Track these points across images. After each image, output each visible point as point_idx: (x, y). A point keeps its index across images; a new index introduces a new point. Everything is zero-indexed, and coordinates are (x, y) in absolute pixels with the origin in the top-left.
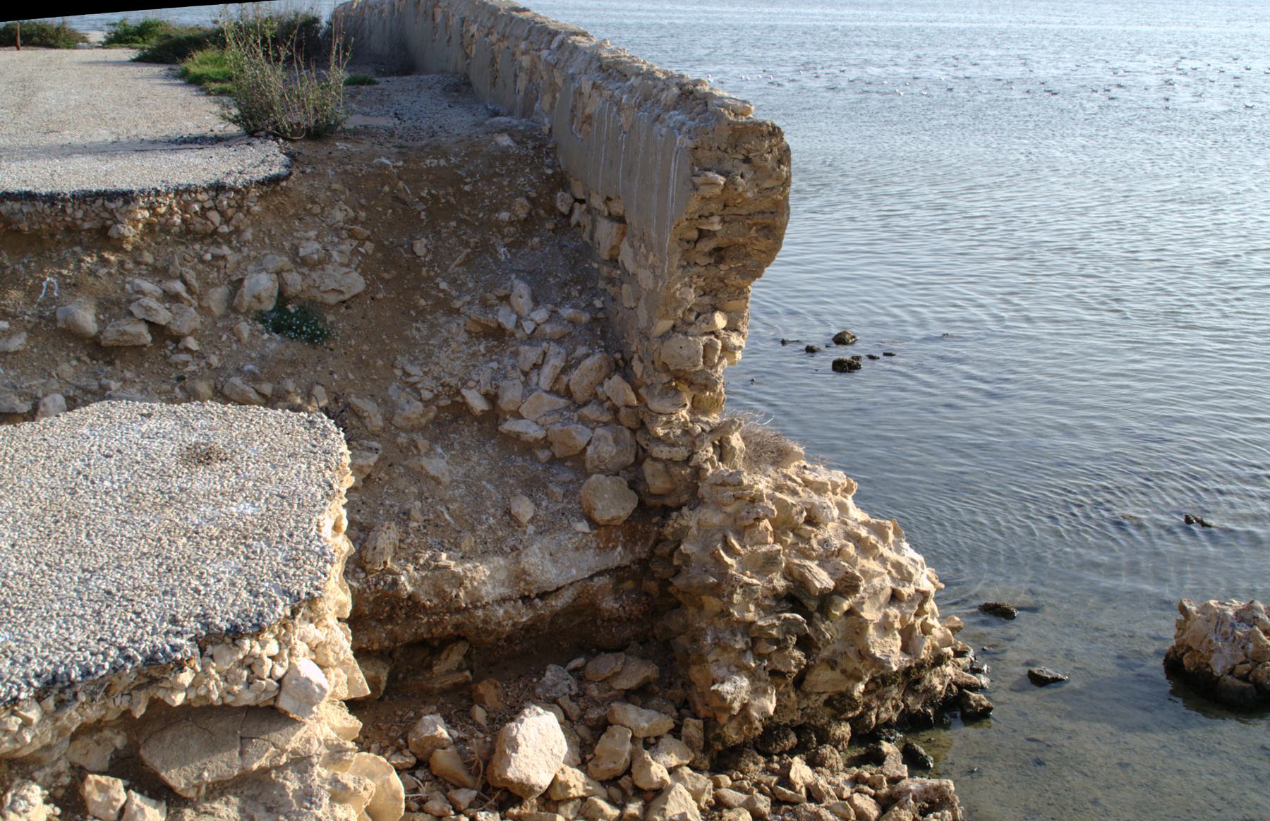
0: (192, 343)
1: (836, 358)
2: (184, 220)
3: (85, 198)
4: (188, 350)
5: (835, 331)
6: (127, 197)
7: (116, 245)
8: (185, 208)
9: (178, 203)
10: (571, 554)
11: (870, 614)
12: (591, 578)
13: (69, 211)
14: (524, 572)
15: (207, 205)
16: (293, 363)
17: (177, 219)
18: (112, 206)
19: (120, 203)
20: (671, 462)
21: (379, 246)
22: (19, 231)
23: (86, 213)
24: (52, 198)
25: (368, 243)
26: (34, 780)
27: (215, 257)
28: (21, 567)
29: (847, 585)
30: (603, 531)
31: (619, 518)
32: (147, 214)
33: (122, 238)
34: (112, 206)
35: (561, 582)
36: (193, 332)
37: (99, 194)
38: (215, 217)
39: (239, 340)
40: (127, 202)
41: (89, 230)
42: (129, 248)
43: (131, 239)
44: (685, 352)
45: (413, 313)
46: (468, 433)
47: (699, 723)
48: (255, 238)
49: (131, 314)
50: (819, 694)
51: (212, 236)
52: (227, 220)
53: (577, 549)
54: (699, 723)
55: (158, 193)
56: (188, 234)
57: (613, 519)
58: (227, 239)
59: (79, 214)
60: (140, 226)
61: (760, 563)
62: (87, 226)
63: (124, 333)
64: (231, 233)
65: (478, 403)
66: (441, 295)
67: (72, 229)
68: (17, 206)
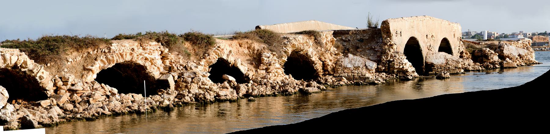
0: (351, 41)
1: (416, 36)
3: (347, 30)
5: (423, 42)
6: (350, 30)
7: (349, 34)
8: (355, 32)
11: (396, 63)
20: (384, 51)
21: (372, 36)
24: (345, 30)
26: (378, 65)
28: (307, 40)
29: (393, 61)
33: (349, 34)
36: (352, 40)
38: (358, 32)
46: (372, 50)
51: (357, 34)
56: (355, 34)
65: (373, 47)
67: (346, 33)
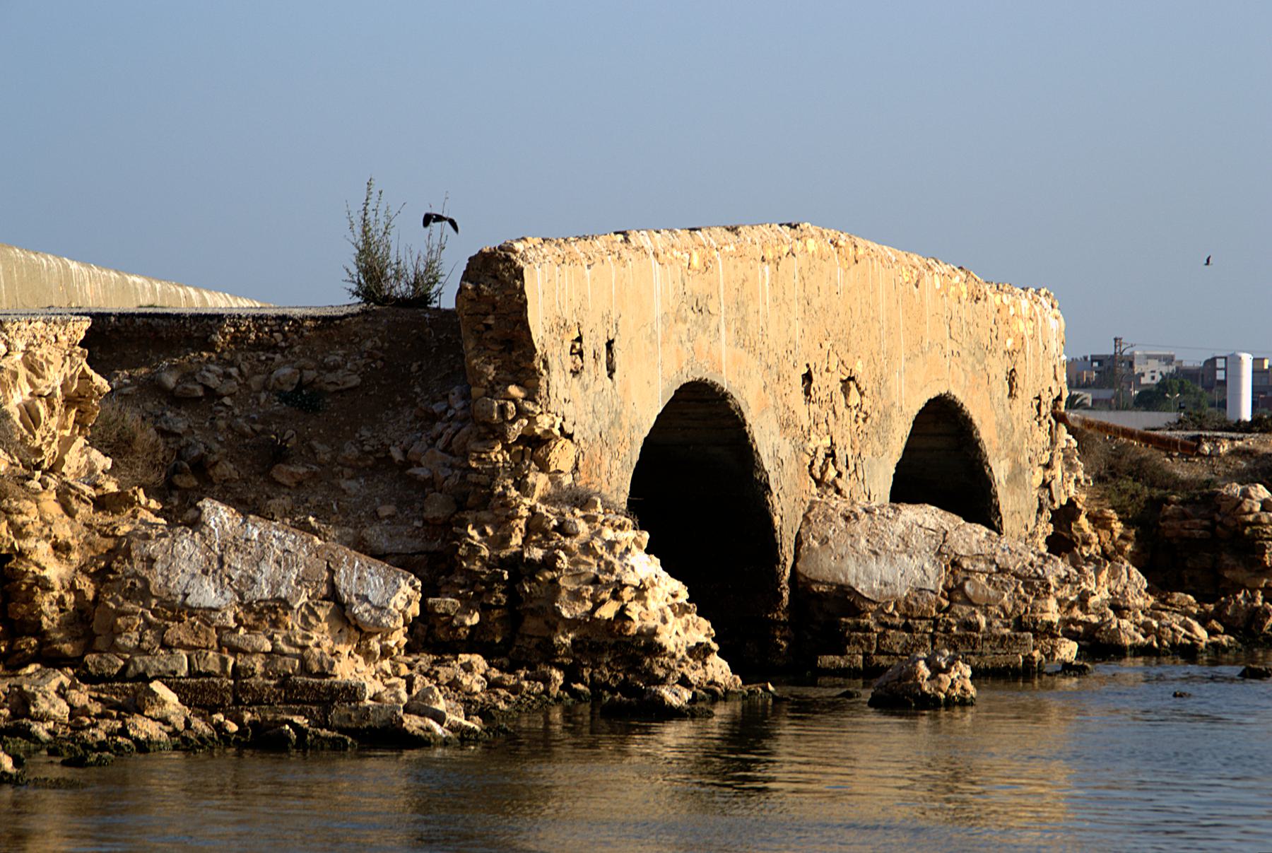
0: (227, 401)
2: (257, 336)
3: (198, 318)
4: (224, 405)
6: (219, 318)
7: (211, 347)
8: (259, 329)
9: (254, 326)
10: (404, 539)
12: (413, 554)
13: (188, 325)
14: (363, 539)
15: (274, 328)
16: (282, 417)
17: (253, 336)
18: (211, 323)
19: (216, 321)
22: (162, 338)
23: (197, 327)
25: (379, 362)
27: (267, 359)
30: (431, 528)
31: (439, 518)
32: (232, 330)
33: (214, 344)
34: (211, 323)
35: (389, 550)
36: (231, 395)
37: (206, 316)
39: (258, 404)
40: (219, 321)
41: (197, 338)
42: (219, 350)
43: (220, 343)
44: (485, 408)
45: (390, 405)
47: (426, 627)
48: (301, 351)
49: (195, 380)
50: (531, 637)
51: (274, 348)
52: (285, 338)
53: (411, 537)
54: (426, 627)
55: (240, 317)
56: (259, 345)
57: (434, 519)
58: (282, 350)
59: (194, 328)
60: (228, 337)
61: (498, 541)
62: (196, 335)
63: (186, 388)
64: (286, 347)
65: (396, 454)
66: (1081, 628)
67: (189, 337)
68: (161, 321)
